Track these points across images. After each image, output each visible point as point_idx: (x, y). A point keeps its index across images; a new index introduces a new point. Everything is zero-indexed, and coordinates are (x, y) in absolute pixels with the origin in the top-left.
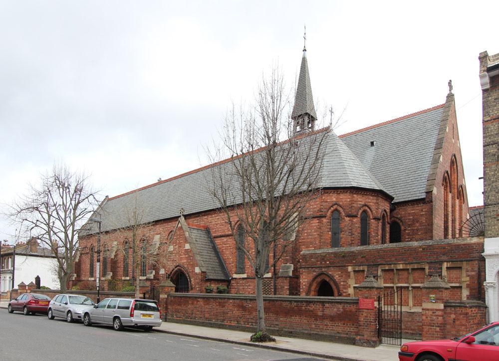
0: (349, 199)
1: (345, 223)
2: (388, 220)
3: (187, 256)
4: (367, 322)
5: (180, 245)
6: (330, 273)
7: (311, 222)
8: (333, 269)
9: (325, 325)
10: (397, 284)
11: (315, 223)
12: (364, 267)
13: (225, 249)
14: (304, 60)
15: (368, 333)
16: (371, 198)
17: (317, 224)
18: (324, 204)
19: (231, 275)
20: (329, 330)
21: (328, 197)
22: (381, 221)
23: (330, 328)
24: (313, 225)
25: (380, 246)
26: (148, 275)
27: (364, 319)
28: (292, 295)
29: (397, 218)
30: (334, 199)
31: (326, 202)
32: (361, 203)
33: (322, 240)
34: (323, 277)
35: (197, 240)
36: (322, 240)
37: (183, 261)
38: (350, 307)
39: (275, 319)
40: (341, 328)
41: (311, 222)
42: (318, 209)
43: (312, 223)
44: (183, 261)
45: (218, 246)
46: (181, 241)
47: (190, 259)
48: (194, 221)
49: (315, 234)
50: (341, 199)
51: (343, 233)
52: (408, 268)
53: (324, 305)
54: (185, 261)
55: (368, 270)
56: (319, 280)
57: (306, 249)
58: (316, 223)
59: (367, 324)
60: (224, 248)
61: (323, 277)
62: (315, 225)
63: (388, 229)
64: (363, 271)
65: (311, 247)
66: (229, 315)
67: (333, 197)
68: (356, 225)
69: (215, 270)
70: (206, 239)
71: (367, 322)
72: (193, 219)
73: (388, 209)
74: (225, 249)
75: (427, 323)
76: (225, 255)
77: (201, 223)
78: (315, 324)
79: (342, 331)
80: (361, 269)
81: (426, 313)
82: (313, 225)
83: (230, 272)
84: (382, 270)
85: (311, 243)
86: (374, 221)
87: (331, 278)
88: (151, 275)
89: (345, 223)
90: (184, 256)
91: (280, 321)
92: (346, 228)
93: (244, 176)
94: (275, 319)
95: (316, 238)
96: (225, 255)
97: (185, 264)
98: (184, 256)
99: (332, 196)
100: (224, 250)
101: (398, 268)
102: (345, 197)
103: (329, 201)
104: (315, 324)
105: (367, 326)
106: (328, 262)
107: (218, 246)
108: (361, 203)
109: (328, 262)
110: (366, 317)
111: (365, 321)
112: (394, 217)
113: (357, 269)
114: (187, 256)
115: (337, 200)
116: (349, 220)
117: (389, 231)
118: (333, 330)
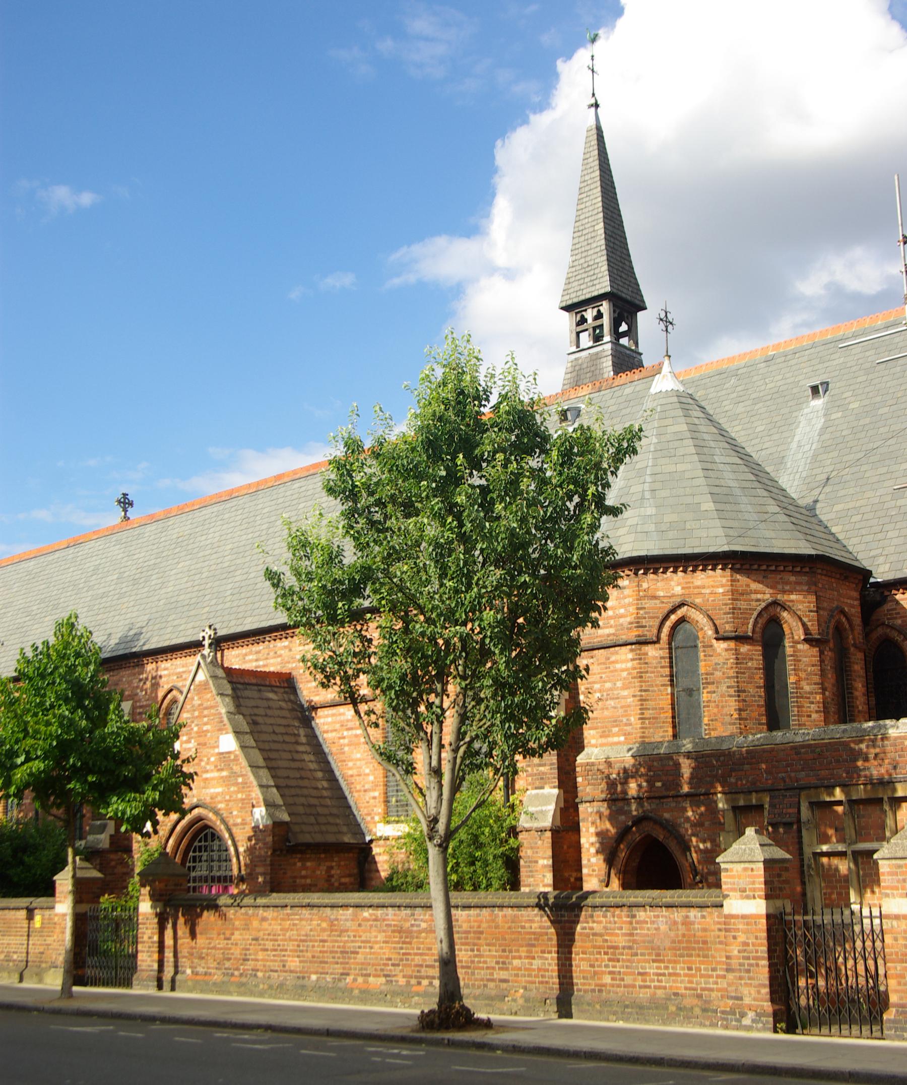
0: (722, 586)
1: (715, 660)
2: (855, 635)
3: (225, 773)
4: (748, 958)
5: (202, 740)
6: (667, 815)
7: (613, 658)
8: (673, 805)
9: (640, 974)
10: (856, 842)
11: (622, 662)
12: (760, 795)
13: (349, 745)
14: (599, 130)
15: (753, 991)
16: (793, 579)
17: (630, 665)
18: (648, 604)
19: (371, 826)
20: (649, 987)
21: (659, 584)
22: (831, 645)
23: (653, 981)
24: (618, 666)
25: (152, 991)
26: (90, 838)
27: (739, 952)
28: (202, 991)
29: (892, 627)
30: (678, 590)
31: (655, 597)
32: (759, 596)
33: (648, 714)
34: (648, 827)
35: (590, 241)
36: (648, 714)
37: (212, 790)
38: (703, 917)
39: (497, 963)
40: (682, 982)
41: (613, 658)
42: (628, 619)
43: (616, 662)
44: (212, 790)
45: (325, 735)
46: (205, 728)
47: (237, 784)
48: (246, 655)
49: (625, 693)
50: (698, 587)
51: (711, 688)
52: (880, 796)
53: (634, 916)
54: (220, 790)
55: (772, 805)
56: (636, 835)
57: (604, 740)
58: (626, 661)
59: (749, 965)
60: (346, 741)
61: (648, 827)
62: (624, 666)
63: (858, 667)
64: (760, 808)
65: (614, 735)
66: (360, 957)
67: (673, 583)
68: (750, 664)
69: (318, 814)
70: (286, 713)
71: (748, 958)
72: (244, 650)
73: (852, 606)
74: (349, 745)
75: (897, 954)
76: (350, 764)
77: (272, 661)
78: (610, 973)
79: (686, 988)
80: (754, 802)
81: (892, 927)
82: (618, 666)
83: (368, 818)
84: (811, 803)
85: (616, 722)
86: (806, 646)
87: (669, 831)
88: (102, 836)
89: (715, 660)
90: (216, 774)
91: (514, 969)
92: (718, 674)
93: (117, 924)
94: (497, 963)
95: (629, 706)
96: (350, 764)
97: (219, 798)
98: (216, 774)
99: (672, 580)
100: (346, 749)
101: (854, 798)
102: (709, 582)
103: (661, 594)
104: (610, 973)
105: (748, 971)
106: (659, 784)
107: (325, 735)
108: (759, 596)
109: (659, 784)
110: (746, 944)
111: (744, 958)
112: (883, 624)
113: (741, 803)
114: (225, 773)
115: (686, 592)
116: (727, 650)
117: (862, 673)
118: (660, 988)
